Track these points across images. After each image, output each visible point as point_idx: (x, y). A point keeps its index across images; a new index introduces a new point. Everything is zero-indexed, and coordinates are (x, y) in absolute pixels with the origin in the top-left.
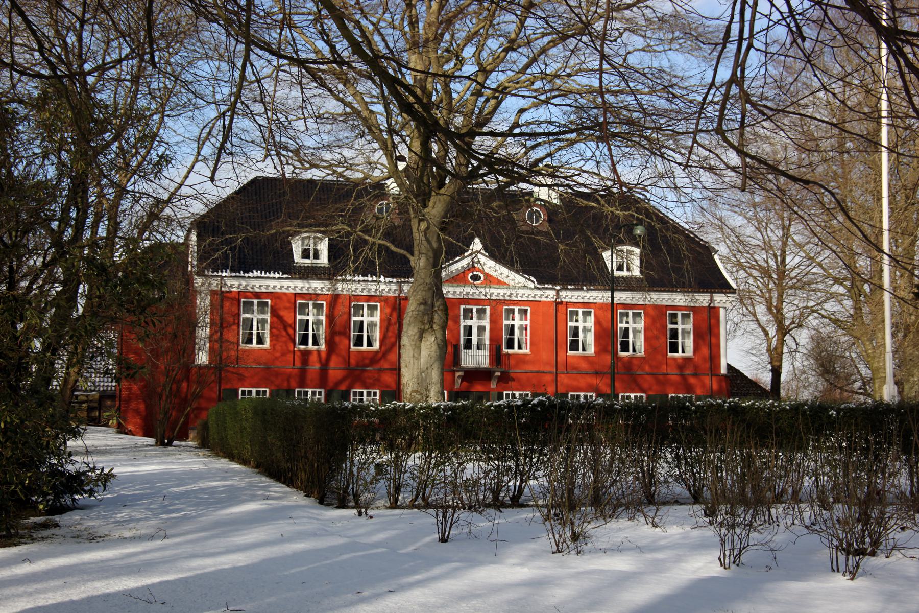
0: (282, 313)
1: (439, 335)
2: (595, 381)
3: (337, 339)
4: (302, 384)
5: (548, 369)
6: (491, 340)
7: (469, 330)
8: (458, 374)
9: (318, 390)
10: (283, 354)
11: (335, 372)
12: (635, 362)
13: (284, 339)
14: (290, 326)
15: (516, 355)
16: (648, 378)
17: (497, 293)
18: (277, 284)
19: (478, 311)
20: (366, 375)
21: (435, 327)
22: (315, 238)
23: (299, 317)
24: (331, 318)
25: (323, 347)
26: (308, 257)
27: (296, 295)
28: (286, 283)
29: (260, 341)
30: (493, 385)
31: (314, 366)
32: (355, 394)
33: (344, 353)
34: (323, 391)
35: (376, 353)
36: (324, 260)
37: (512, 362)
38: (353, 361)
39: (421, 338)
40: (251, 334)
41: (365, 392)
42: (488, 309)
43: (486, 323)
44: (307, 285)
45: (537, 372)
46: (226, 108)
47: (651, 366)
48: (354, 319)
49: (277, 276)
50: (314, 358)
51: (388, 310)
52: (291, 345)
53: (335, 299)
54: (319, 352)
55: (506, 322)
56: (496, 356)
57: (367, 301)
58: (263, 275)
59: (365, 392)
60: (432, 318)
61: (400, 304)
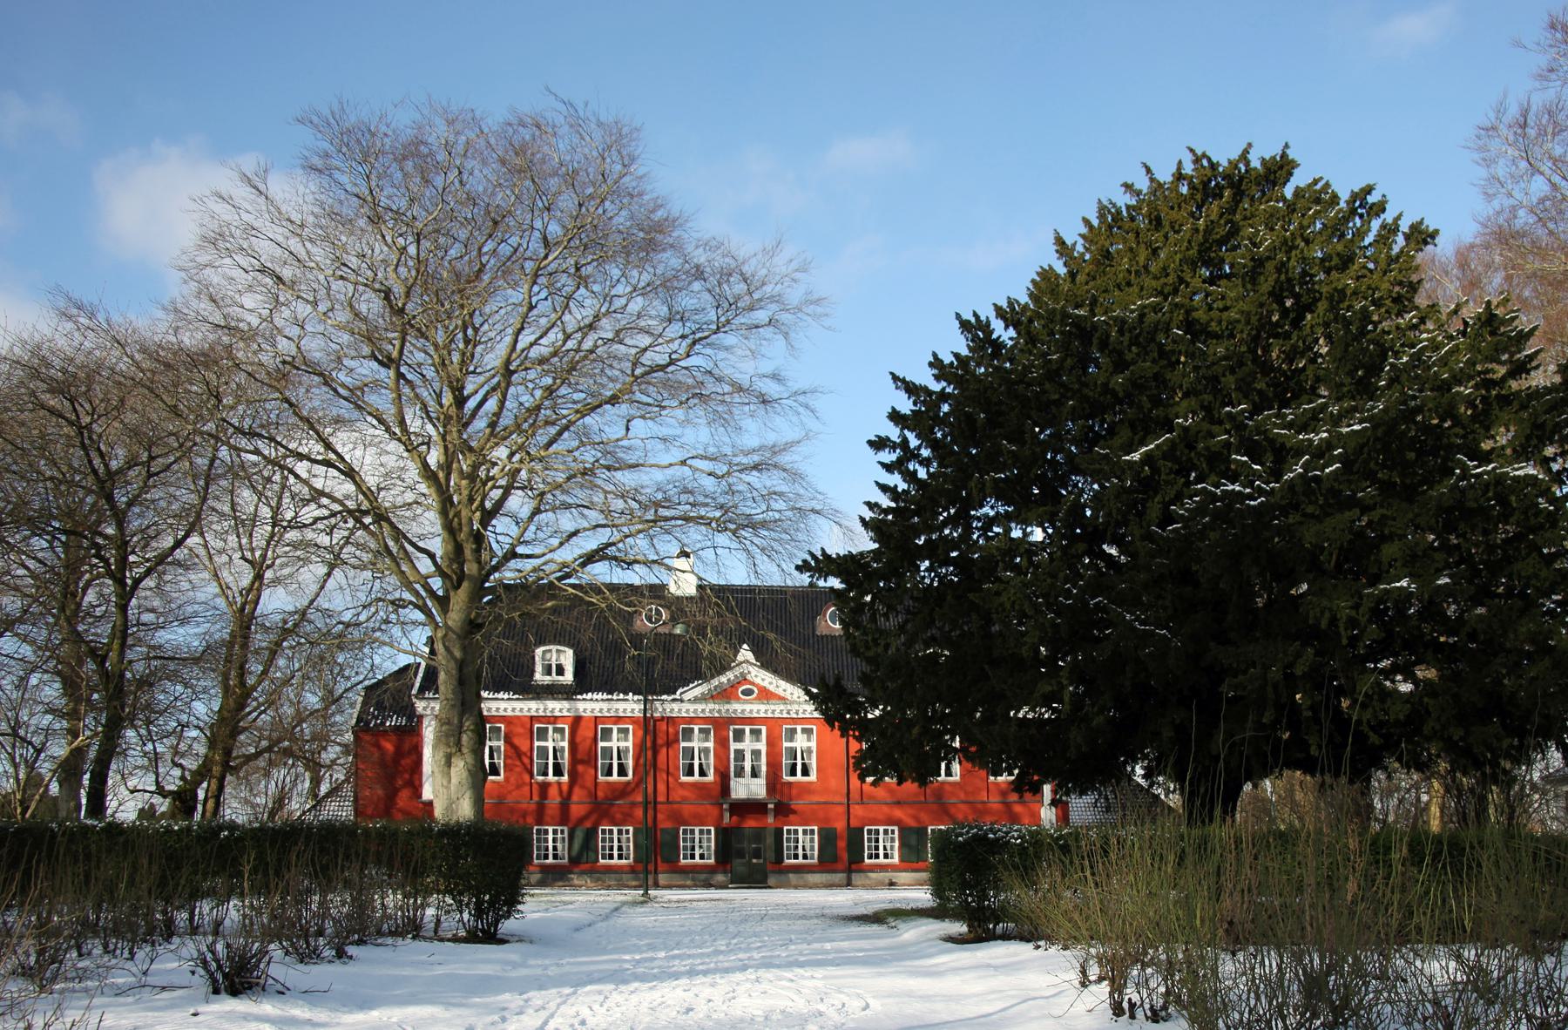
0: (517, 741)
1: (470, 758)
2: (898, 813)
3: (580, 768)
4: (540, 822)
5: (837, 799)
6: (768, 764)
7: (740, 755)
8: (725, 806)
9: (559, 828)
10: (518, 787)
11: (577, 809)
12: (947, 787)
14: (525, 754)
15: (799, 784)
16: (962, 807)
17: (775, 710)
18: (509, 705)
19: (752, 731)
21: (465, 750)
22: (558, 651)
23: (537, 744)
24: (572, 743)
26: (549, 674)
27: (532, 718)
28: (518, 705)
29: (805, 772)
30: (771, 820)
31: (554, 799)
32: (604, 832)
33: (589, 784)
34: (566, 829)
35: (628, 783)
36: (568, 677)
37: (794, 792)
38: (600, 794)
39: (449, 764)
40: (611, 764)
41: (615, 829)
42: (764, 729)
43: (762, 746)
44: (542, 707)
45: (825, 803)
46: (278, 473)
48: (601, 744)
49: (506, 696)
50: (553, 791)
51: (640, 733)
52: (526, 777)
53: (577, 721)
54: (559, 784)
55: (786, 744)
56: (774, 783)
57: (615, 723)
58: (491, 696)
59: (615, 829)
61: (655, 726)
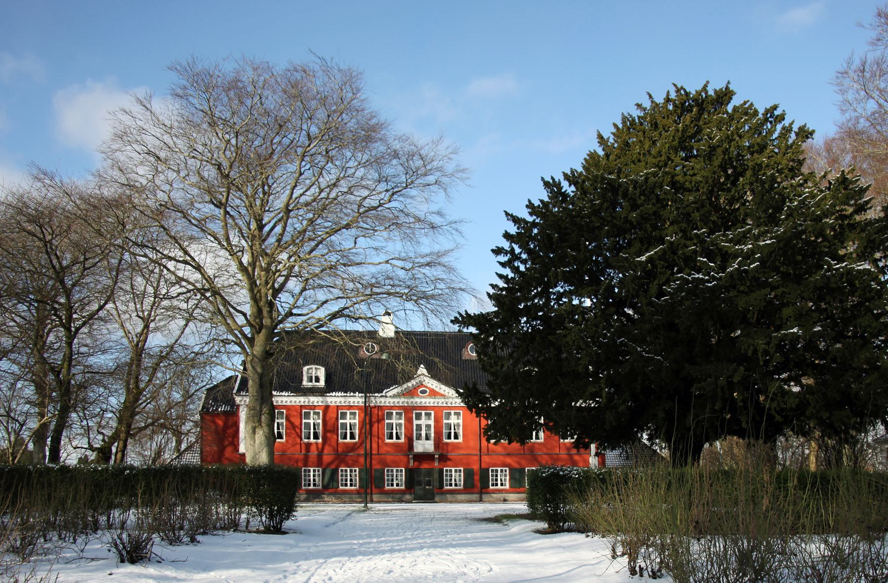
0: (293, 420)
1: (266, 429)
3: (329, 435)
5: (474, 452)
6: (435, 433)
7: (419, 427)
8: (410, 456)
9: (317, 469)
10: (293, 445)
11: (327, 458)
12: (536, 446)
13: (293, 436)
15: (452, 443)
16: (545, 456)
17: (439, 402)
18: (288, 399)
19: (426, 414)
20: (348, 458)
21: (263, 425)
22: (316, 368)
23: (304, 421)
25: (320, 441)
27: (301, 406)
28: (294, 399)
29: (456, 437)
30: (436, 464)
31: (314, 452)
32: (342, 471)
33: (334, 444)
34: (320, 469)
35: (356, 443)
36: (322, 383)
37: (450, 448)
38: (340, 449)
39: (254, 432)
40: (346, 433)
41: (348, 469)
42: (433, 413)
43: (432, 422)
44: (307, 400)
45: (467, 455)
46: (158, 268)
47: (547, 449)
48: (340, 421)
49: (287, 394)
50: (313, 448)
52: (298, 440)
53: (327, 408)
54: (317, 444)
55: (445, 421)
56: (438, 443)
57: (348, 409)
58: (278, 394)
59: (348, 469)
60: (260, 419)
61: (371, 411)
